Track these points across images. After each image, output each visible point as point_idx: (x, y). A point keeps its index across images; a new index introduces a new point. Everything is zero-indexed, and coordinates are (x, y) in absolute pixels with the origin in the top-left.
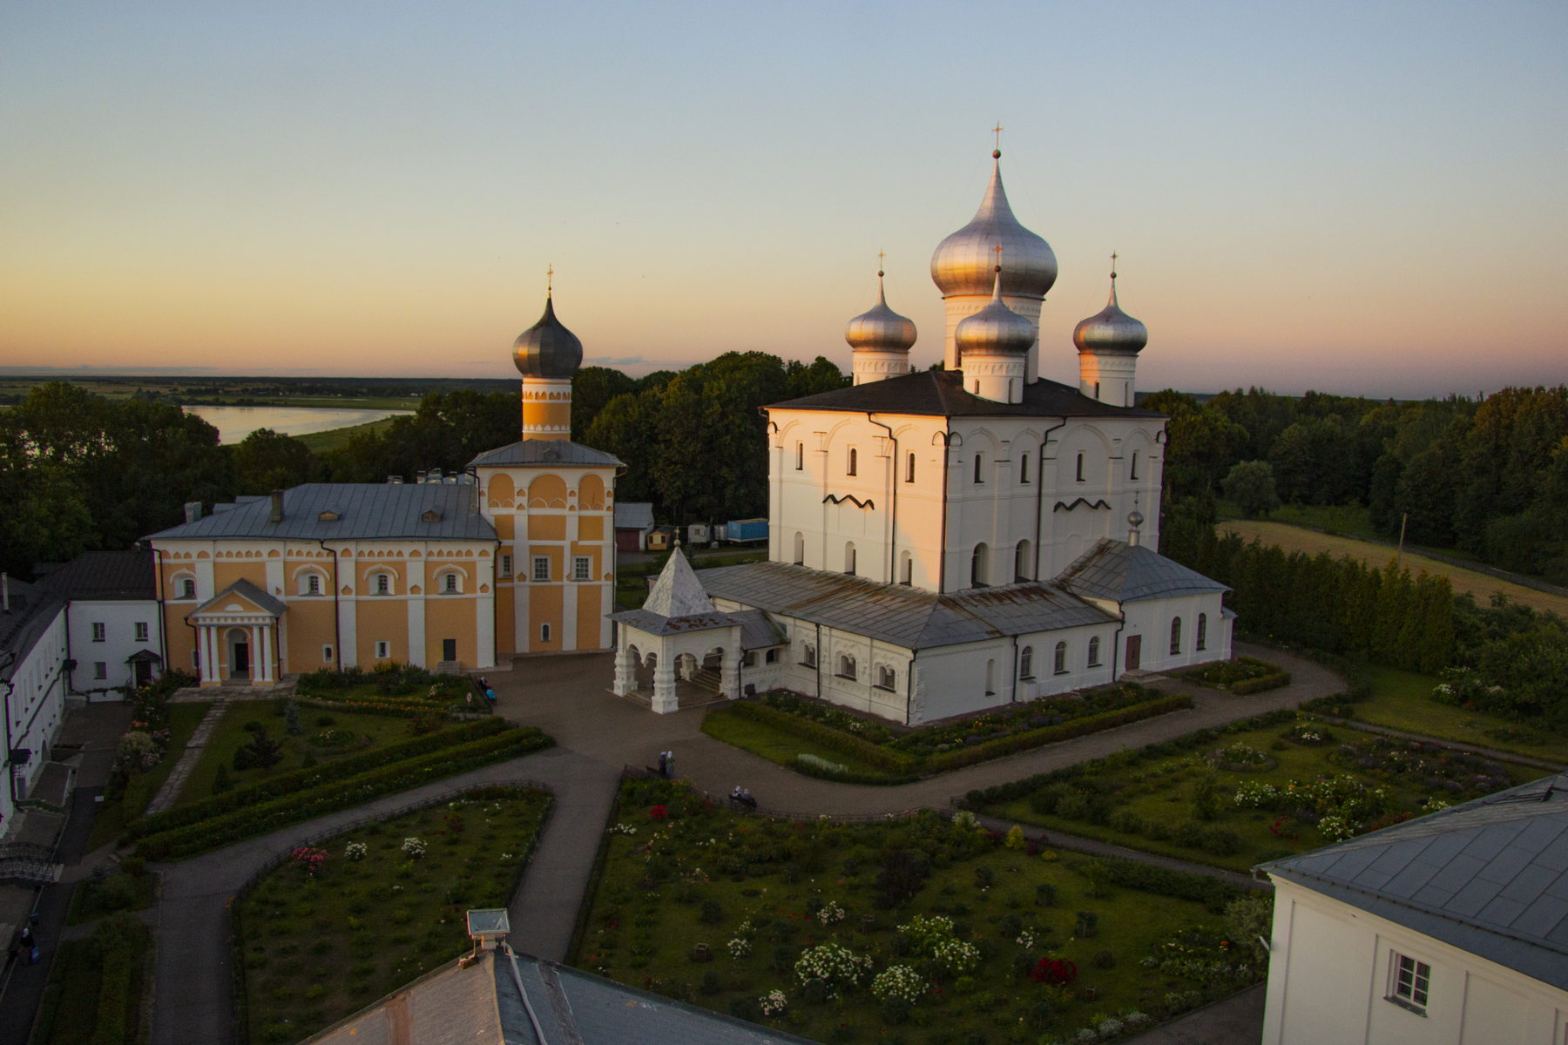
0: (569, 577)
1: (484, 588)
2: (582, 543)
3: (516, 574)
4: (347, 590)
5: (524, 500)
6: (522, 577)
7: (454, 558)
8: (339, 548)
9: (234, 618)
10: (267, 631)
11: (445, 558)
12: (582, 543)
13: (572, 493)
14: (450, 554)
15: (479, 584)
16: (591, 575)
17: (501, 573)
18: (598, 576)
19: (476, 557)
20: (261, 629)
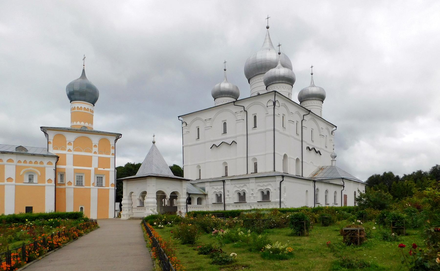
0: (93, 184)
1: (49, 181)
2: (99, 169)
3: (67, 182)
5: (71, 147)
6: (70, 183)
7: (33, 165)
12: (99, 169)
13: (95, 146)
14: (31, 162)
15: (47, 178)
16: (104, 185)
17: (59, 181)
18: (107, 185)
19: (45, 164)
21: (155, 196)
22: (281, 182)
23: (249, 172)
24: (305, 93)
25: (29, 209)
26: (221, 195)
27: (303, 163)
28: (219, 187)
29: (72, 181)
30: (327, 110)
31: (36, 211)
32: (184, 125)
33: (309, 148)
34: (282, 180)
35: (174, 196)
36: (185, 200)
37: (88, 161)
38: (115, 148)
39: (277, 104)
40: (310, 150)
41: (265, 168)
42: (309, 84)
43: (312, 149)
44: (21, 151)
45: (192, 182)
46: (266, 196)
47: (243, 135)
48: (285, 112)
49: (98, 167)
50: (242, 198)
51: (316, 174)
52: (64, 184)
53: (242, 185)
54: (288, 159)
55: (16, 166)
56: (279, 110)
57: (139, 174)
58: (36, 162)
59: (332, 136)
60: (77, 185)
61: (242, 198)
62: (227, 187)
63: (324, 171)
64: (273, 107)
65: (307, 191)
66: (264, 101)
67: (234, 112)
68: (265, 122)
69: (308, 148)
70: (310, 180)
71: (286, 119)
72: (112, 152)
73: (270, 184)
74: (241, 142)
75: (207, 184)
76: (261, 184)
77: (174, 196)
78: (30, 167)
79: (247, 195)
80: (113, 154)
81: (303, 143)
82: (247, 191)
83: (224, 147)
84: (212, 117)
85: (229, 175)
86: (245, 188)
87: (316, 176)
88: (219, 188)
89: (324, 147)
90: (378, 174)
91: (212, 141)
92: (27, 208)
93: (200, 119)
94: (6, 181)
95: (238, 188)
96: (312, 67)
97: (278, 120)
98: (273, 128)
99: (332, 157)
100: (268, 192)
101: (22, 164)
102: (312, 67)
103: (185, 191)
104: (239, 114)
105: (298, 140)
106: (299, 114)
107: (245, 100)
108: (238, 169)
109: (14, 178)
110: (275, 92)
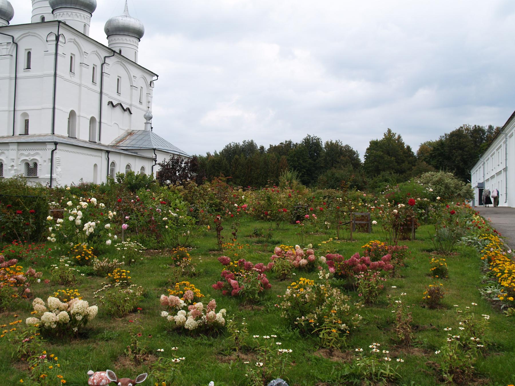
22: (53, 151)
23: (17, 133)
24: (115, 24)
27: (102, 125)
33: (112, 103)
34: (54, 148)
39: (61, 39)
40: (113, 106)
41: (39, 128)
47: (10, 79)
48: (76, 52)
50: (32, 169)
51: (121, 141)
54: (77, 117)
56: (67, 48)
59: (151, 88)
63: (133, 137)
64: (55, 43)
65: (95, 165)
66: (43, 32)
68: (43, 63)
69: (111, 103)
71: (77, 61)
73: (37, 154)
76: (26, 153)
81: (103, 96)
87: (121, 144)
89: (136, 103)
97: (63, 63)
98: (53, 72)
99: (145, 118)
104: (5, 47)
105: (95, 91)
106: (98, 55)
107: (20, 27)
110: (59, 22)
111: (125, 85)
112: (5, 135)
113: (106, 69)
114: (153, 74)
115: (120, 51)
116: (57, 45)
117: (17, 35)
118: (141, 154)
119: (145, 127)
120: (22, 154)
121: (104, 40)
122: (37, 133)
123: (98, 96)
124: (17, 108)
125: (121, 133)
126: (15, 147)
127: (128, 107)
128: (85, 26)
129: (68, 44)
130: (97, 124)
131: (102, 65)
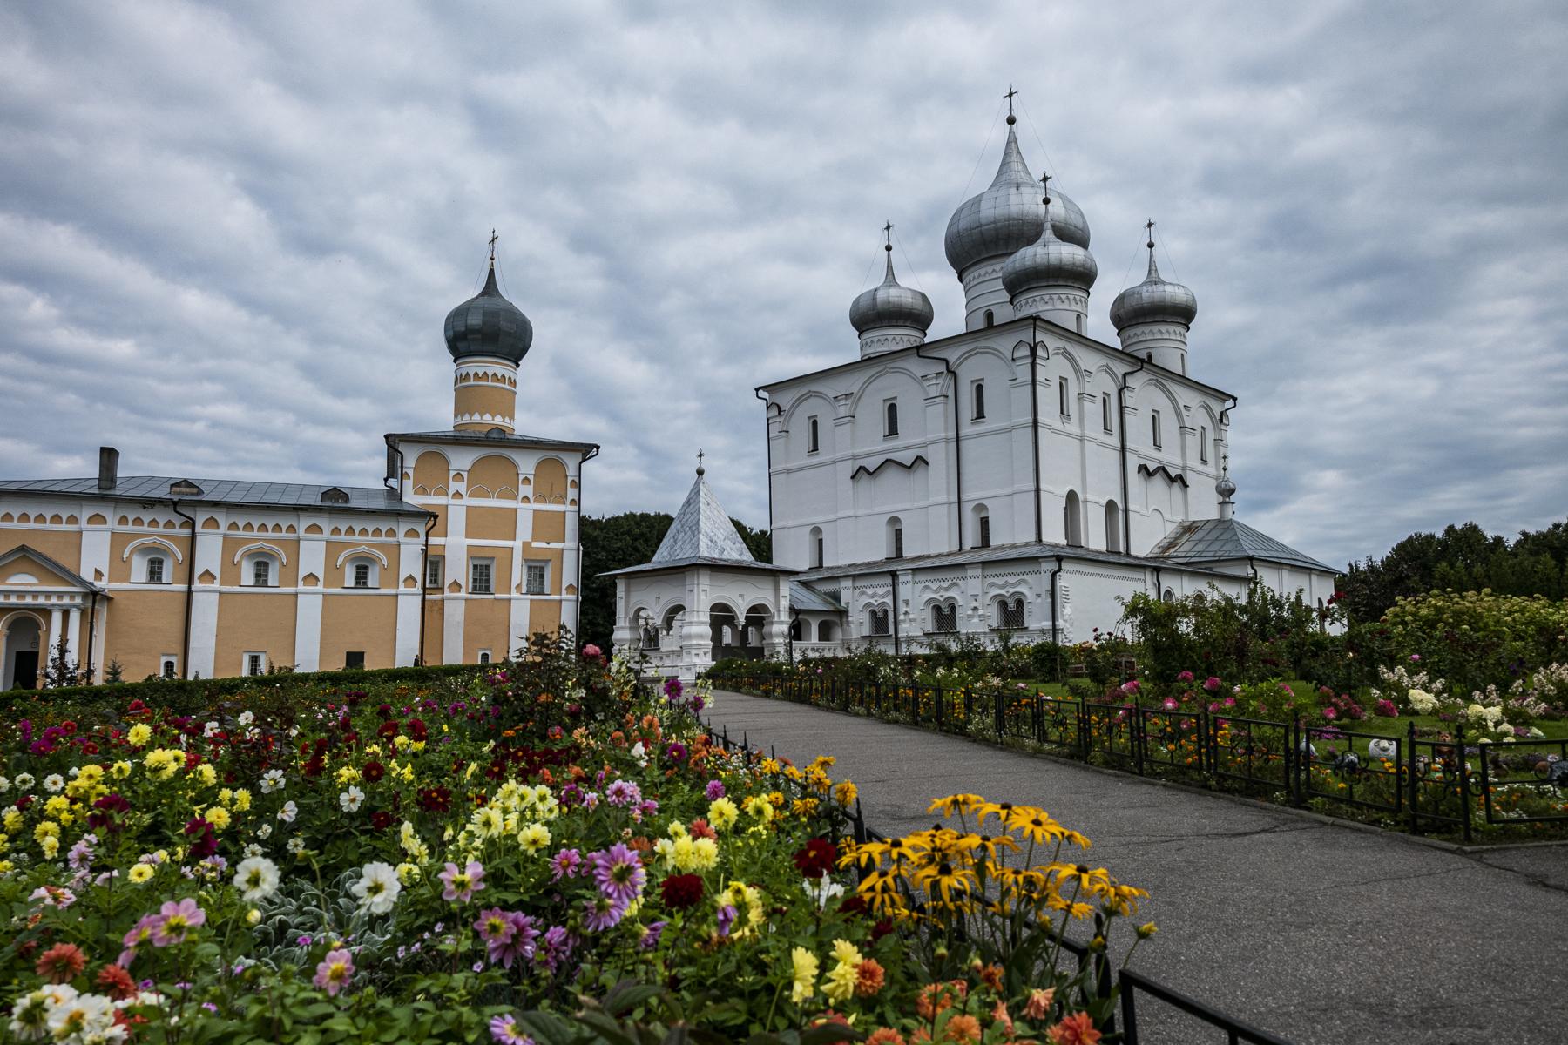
0: (519, 587)
2: (535, 544)
3: (448, 582)
4: (208, 575)
5: (461, 487)
6: (456, 586)
7: (270, 534)
8: (200, 518)
9: (21, 595)
10: (75, 617)
11: (357, 538)
12: (535, 544)
13: (526, 480)
14: (364, 532)
16: (547, 589)
19: (401, 537)
20: (66, 614)
21: (708, 620)
22: (1054, 575)
23: (968, 545)
24: (1132, 302)
25: (355, 658)
26: (886, 612)
27: (1131, 515)
28: (881, 591)
29: (462, 582)
30: (1194, 350)
31: (369, 666)
32: (774, 412)
35: (758, 616)
36: (785, 628)
37: (505, 523)
38: (577, 484)
39: (1040, 352)
41: (1010, 533)
42: (1143, 277)
43: (1157, 470)
44: (335, 502)
45: (803, 578)
46: (1013, 614)
47: (947, 441)
49: (535, 539)
52: (441, 590)
53: (945, 585)
55: (225, 539)
56: (1052, 368)
57: (661, 557)
58: (377, 532)
60: (475, 590)
61: (945, 617)
62: (905, 591)
64: (1029, 360)
66: (1005, 344)
67: (919, 374)
68: (1007, 405)
69: (1143, 469)
70: (1144, 567)
72: (570, 497)
73: (1024, 581)
74: (940, 459)
75: (848, 583)
76: (1000, 581)
77: (758, 616)
78: (359, 544)
79: (959, 613)
80: (573, 502)
81: (1129, 455)
82: (960, 601)
83: (891, 475)
84: (855, 389)
85: (907, 553)
86: (953, 593)
88: (878, 593)
89: (1193, 461)
90: (1425, 532)
91: (854, 458)
92: (349, 655)
93: (820, 395)
94: (300, 582)
95: (936, 591)
96: (1150, 225)
97: (1048, 398)
98: (1030, 419)
100: (1020, 603)
101: (343, 537)
102: (1150, 225)
103: (785, 604)
105: (1110, 447)
108: (932, 536)
109: (321, 575)
111: (1169, 425)
112: (945, 550)
113: (1129, 400)
114: (1223, 396)
115: (1150, 357)
116: (1033, 365)
117: (953, 355)
118: (1218, 570)
119: (1222, 512)
120: (992, 585)
121: (1110, 337)
122: (1007, 541)
123: (1116, 455)
124: (964, 497)
125: (1170, 529)
126: (978, 571)
127: (1179, 472)
128: (1078, 317)
129: (1053, 359)
130: (1121, 515)
131: (1120, 392)
